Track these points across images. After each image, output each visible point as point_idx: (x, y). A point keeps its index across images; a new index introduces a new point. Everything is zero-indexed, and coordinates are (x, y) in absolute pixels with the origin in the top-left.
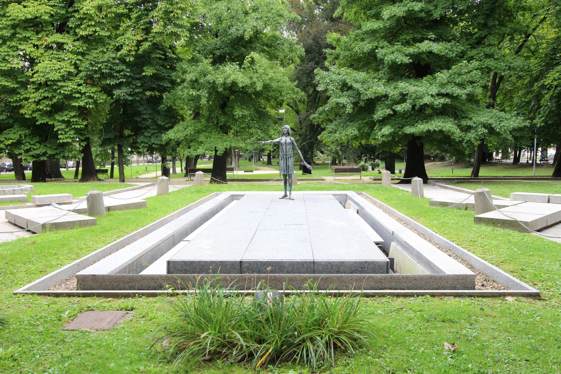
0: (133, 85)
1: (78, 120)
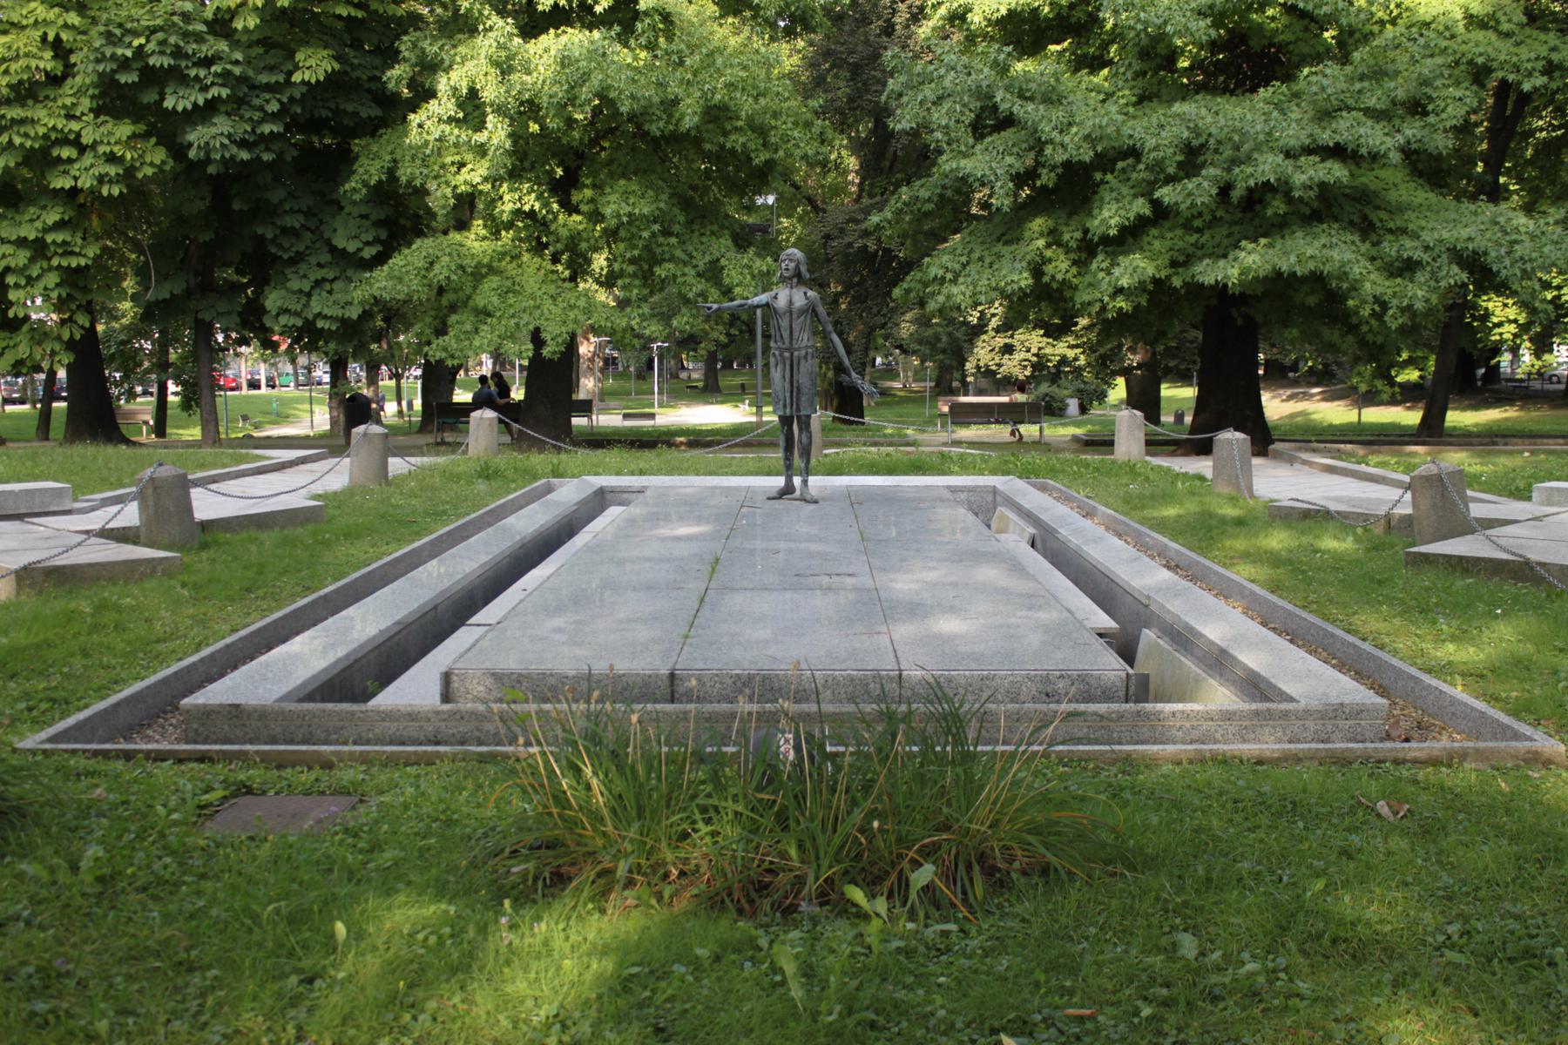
1: (69, 239)
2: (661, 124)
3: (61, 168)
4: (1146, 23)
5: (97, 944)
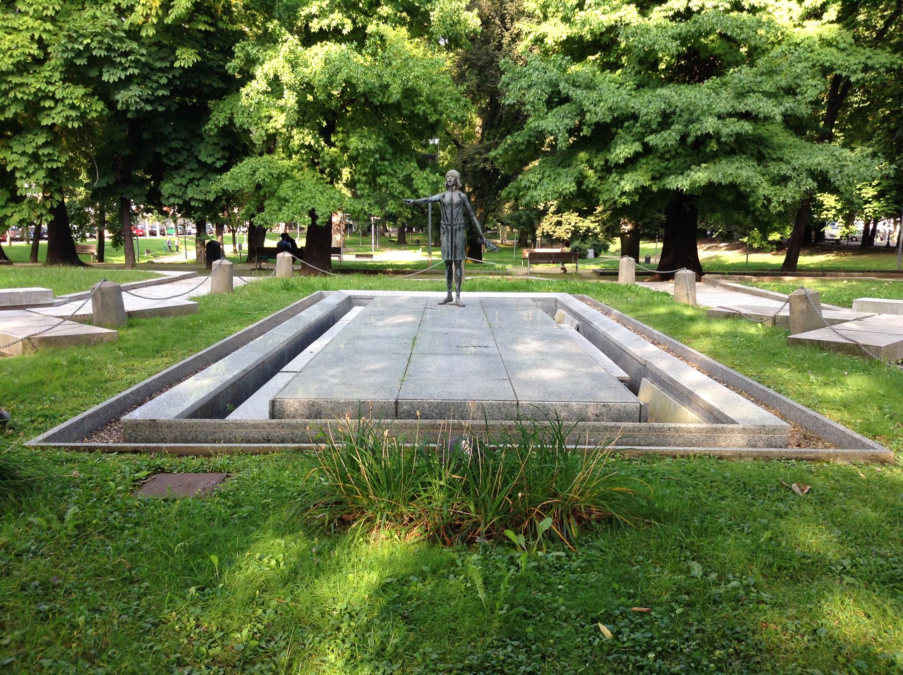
0: (153, 81)
1: (51, 152)
2: (380, 98)
3: (46, 113)
4: (644, 44)
5: (77, 567)
